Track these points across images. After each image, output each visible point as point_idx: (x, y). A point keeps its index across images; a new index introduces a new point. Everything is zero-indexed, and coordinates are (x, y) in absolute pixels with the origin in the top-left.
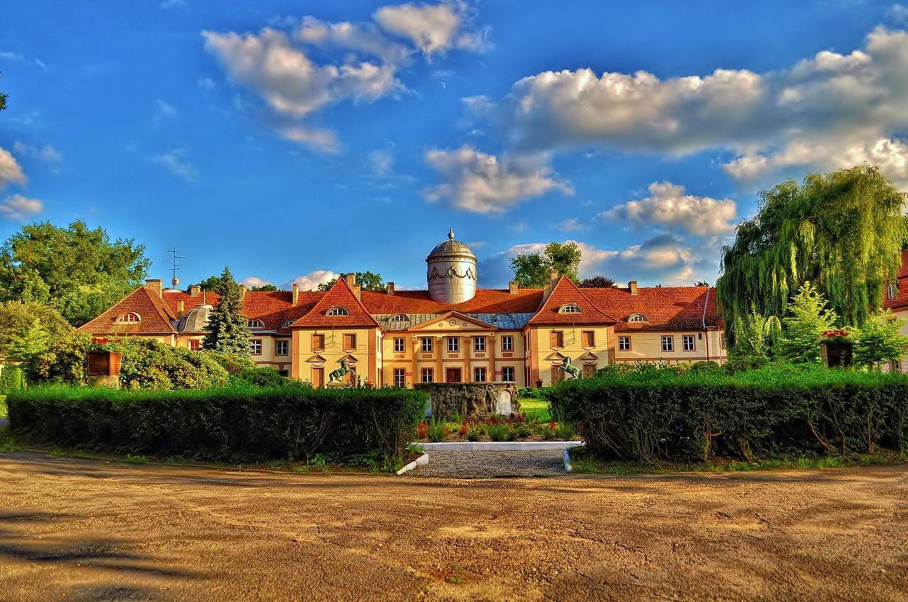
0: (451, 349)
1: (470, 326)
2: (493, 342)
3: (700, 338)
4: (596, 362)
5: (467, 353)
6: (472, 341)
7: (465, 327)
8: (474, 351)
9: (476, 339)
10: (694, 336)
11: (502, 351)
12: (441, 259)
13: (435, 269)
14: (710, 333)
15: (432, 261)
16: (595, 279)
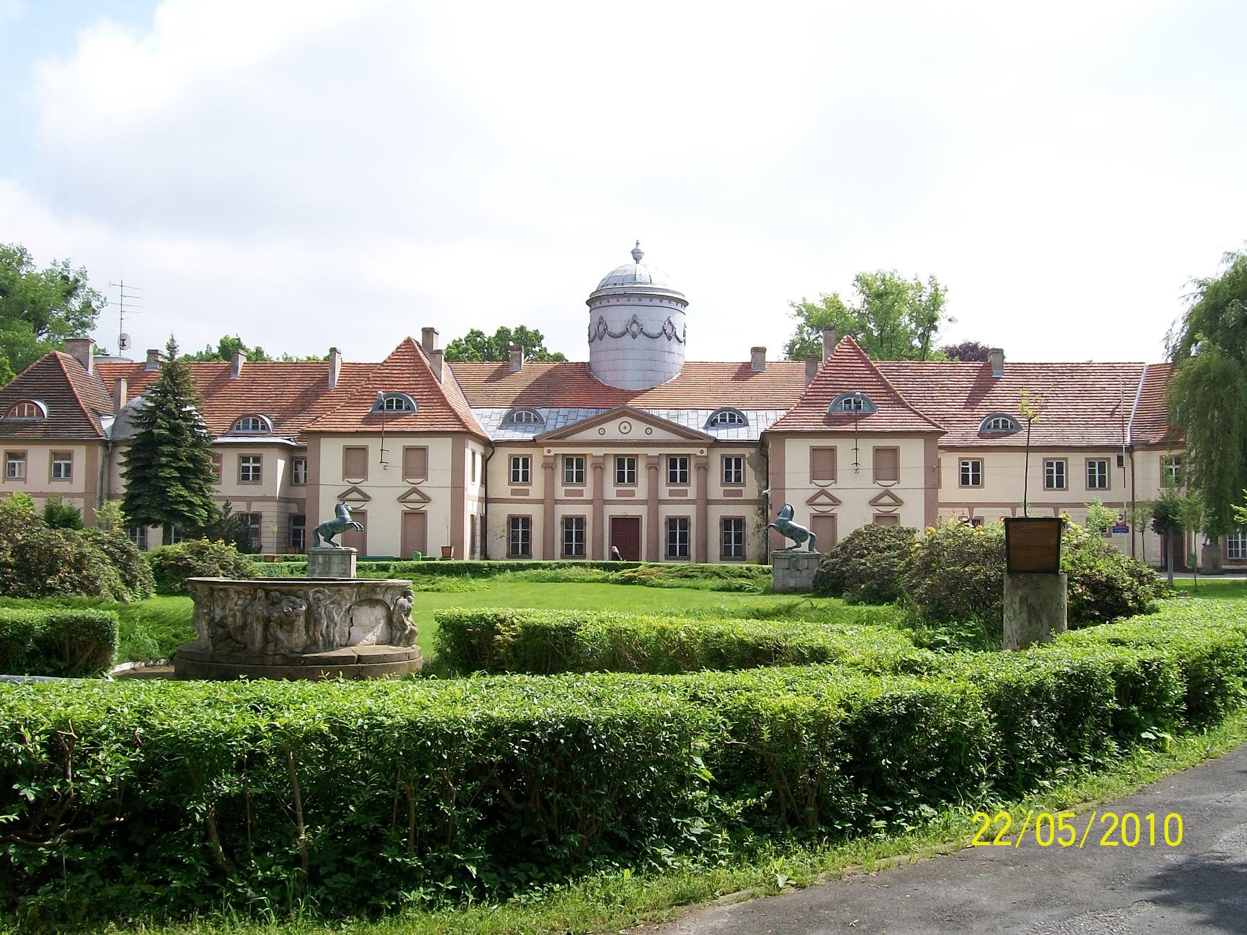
0: (516, 478)
1: (659, 434)
2: (704, 467)
4: (836, 510)
5: (549, 486)
6: (560, 463)
8: (564, 484)
10: (1108, 459)
11: (510, 484)
12: (613, 301)
13: (601, 321)
15: (598, 304)
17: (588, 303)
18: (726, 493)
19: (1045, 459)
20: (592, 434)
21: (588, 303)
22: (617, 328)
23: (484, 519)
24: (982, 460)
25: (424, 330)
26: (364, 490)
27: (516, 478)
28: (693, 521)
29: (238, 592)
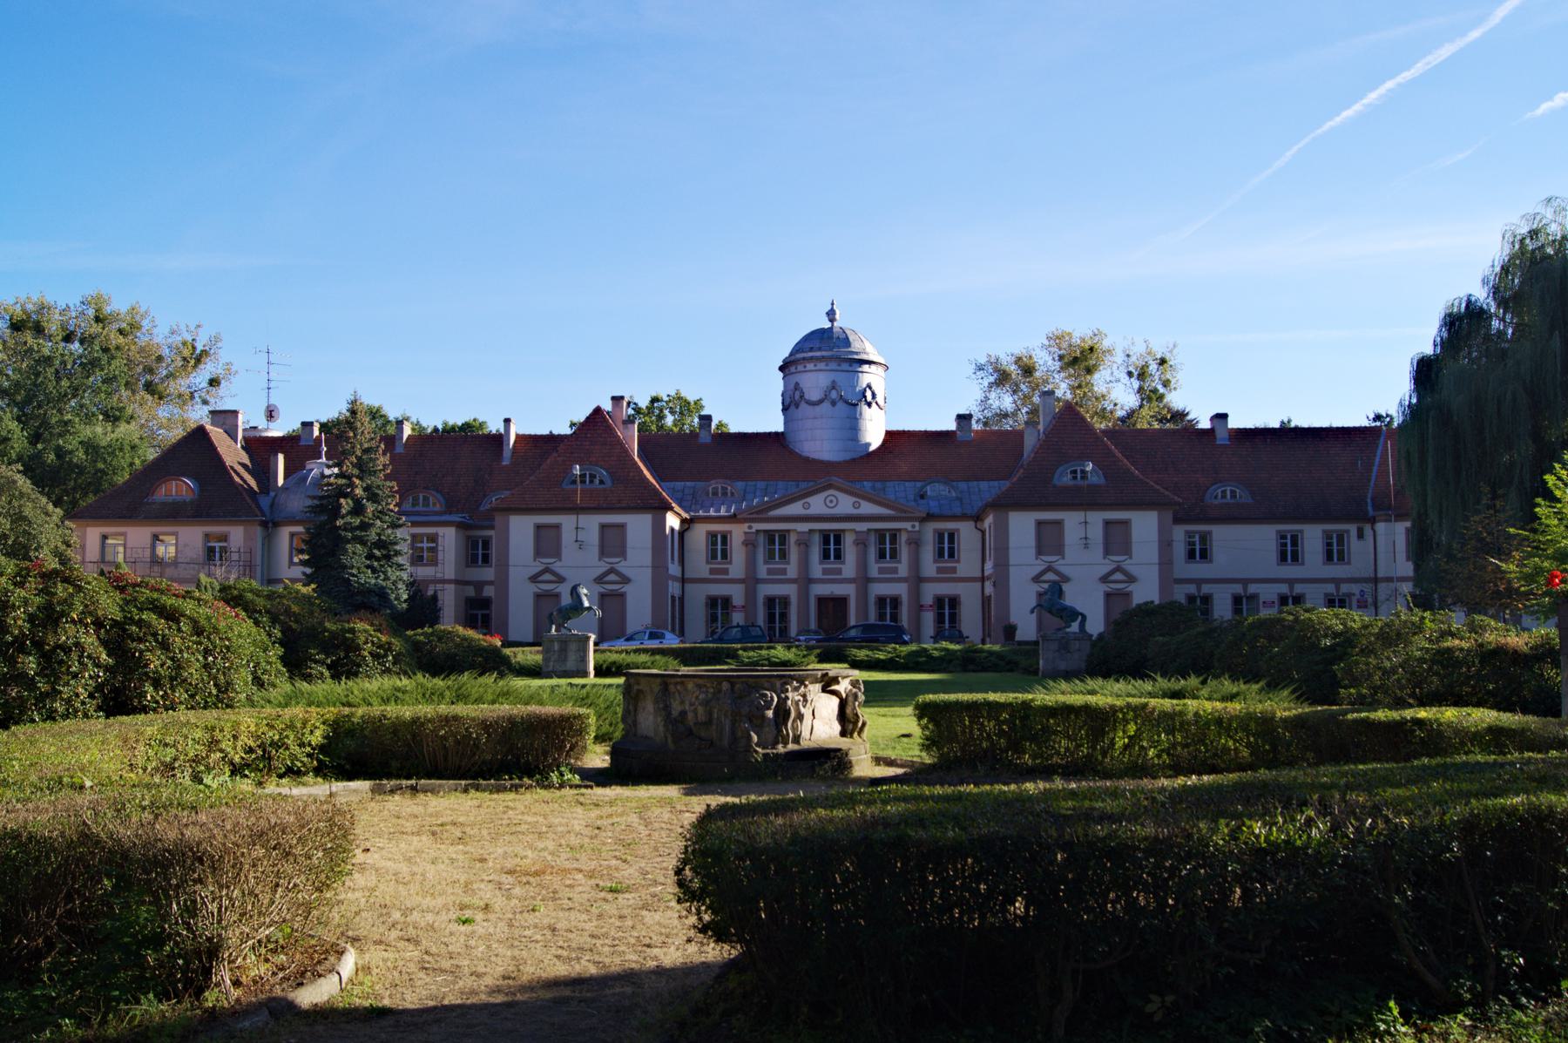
0: (714, 557)
1: (868, 508)
2: (916, 543)
3: (1360, 535)
4: (626, 588)
7: (855, 512)
8: (766, 562)
9: (881, 534)
10: (1348, 531)
14: (1381, 527)
15: (793, 369)
16: (338, 433)
17: (781, 369)
18: (939, 570)
19: (1278, 532)
20: (795, 509)
21: (781, 369)
22: (814, 395)
23: (682, 599)
24: (1210, 533)
25: (614, 398)
26: (1062, 569)
27: (714, 557)
28: (905, 599)
29: (699, 686)
